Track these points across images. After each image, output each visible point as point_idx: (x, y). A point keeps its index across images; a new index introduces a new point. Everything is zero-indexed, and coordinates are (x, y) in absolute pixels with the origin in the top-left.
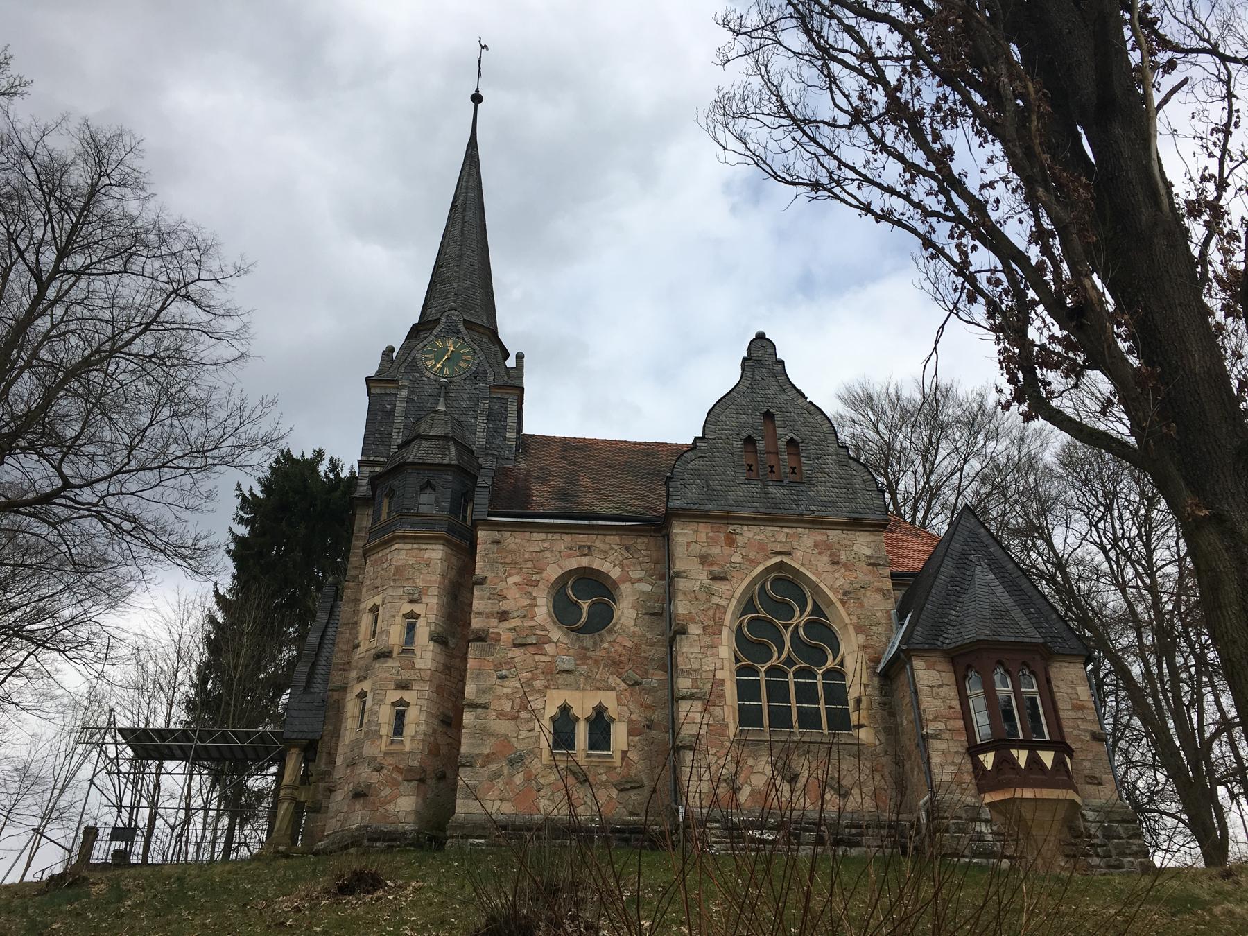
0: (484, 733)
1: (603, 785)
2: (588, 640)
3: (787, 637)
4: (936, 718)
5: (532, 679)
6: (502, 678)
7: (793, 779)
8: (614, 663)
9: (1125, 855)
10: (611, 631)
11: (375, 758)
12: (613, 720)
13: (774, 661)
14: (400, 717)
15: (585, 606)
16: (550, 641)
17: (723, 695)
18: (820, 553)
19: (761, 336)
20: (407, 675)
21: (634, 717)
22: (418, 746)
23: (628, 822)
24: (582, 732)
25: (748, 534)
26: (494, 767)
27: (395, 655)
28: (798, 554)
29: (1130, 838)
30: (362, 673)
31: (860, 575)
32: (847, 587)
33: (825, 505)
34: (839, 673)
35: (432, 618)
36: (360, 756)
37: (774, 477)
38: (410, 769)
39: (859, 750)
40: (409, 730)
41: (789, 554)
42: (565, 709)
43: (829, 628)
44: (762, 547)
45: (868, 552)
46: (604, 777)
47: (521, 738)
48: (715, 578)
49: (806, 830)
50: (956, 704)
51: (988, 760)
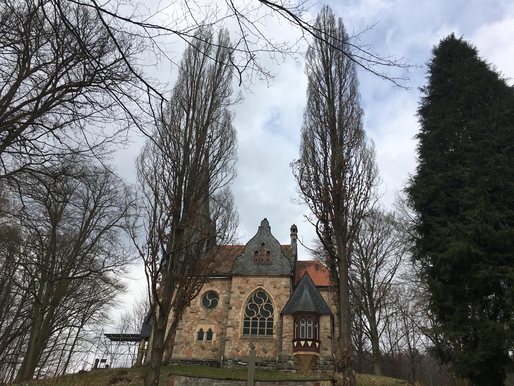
0: (181, 336)
1: (208, 350)
2: (209, 310)
3: (259, 309)
4: (286, 332)
5: (194, 322)
6: (186, 321)
10: (215, 308)
15: (210, 301)
16: (200, 311)
17: (239, 326)
19: (265, 219)
21: (218, 332)
23: (212, 360)
24: (205, 336)
25: (252, 280)
26: (182, 345)
28: (265, 285)
29: (331, 365)
32: (277, 295)
33: (274, 270)
34: (272, 319)
37: (262, 263)
41: (262, 285)
42: (201, 330)
43: (271, 306)
44: (255, 284)
45: (284, 284)
46: (209, 348)
47: (189, 338)
48: (241, 293)
50: (292, 328)
51: (295, 343)
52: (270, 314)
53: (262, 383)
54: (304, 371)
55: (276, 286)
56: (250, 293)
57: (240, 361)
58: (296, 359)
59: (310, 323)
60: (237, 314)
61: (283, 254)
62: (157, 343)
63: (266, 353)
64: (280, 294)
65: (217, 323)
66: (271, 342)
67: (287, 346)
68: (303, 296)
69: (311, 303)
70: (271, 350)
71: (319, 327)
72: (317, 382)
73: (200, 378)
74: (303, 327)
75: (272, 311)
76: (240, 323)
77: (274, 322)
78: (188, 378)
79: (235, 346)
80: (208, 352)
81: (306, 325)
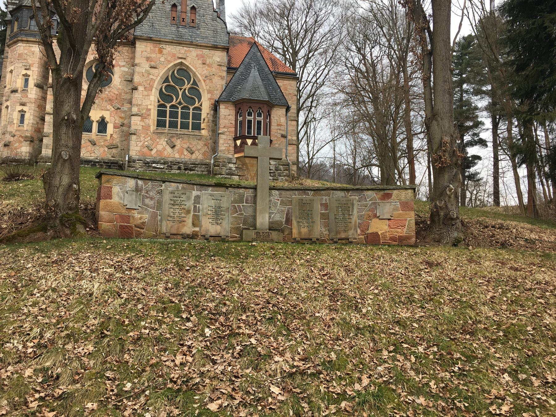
1: (102, 146)
3: (180, 93)
7: (173, 147)
8: (110, 100)
9: (280, 176)
10: (109, 87)
11: (12, 132)
12: (108, 122)
13: (174, 103)
14: (23, 116)
18: (198, 59)
20: (24, 100)
21: (117, 121)
22: (30, 128)
23: (111, 160)
25: (168, 49)
27: (19, 91)
28: (189, 59)
30: (7, 98)
31: (214, 69)
32: (207, 74)
34: (199, 109)
35: (35, 77)
36: (6, 131)
37: (183, 24)
38: (26, 137)
39: (200, 138)
40: (26, 122)
43: (198, 91)
44: (174, 55)
45: (218, 60)
46: (103, 143)
49: (175, 165)
50: (234, 122)
51: (238, 142)
52: (197, 102)
53: (283, 192)
54: (250, 177)
55: (206, 61)
56: (166, 69)
57: (154, 162)
58: (238, 162)
59: (259, 115)
60: (146, 98)
61: (216, 14)
62: (67, 108)
63: (192, 154)
64: (212, 74)
65: (113, 109)
66: (199, 140)
67: (227, 145)
68: (250, 79)
69: (262, 89)
70: (199, 150)
71: (270, 122)
72: (386, 192)
73: (164, 182)
74: (250, 122)
75: (200, 98)
76: (152, 111)
77: (203, 112)
78: (140, 182)
79: (146, 143)
80: (102, 150)
81: (255, 118)
